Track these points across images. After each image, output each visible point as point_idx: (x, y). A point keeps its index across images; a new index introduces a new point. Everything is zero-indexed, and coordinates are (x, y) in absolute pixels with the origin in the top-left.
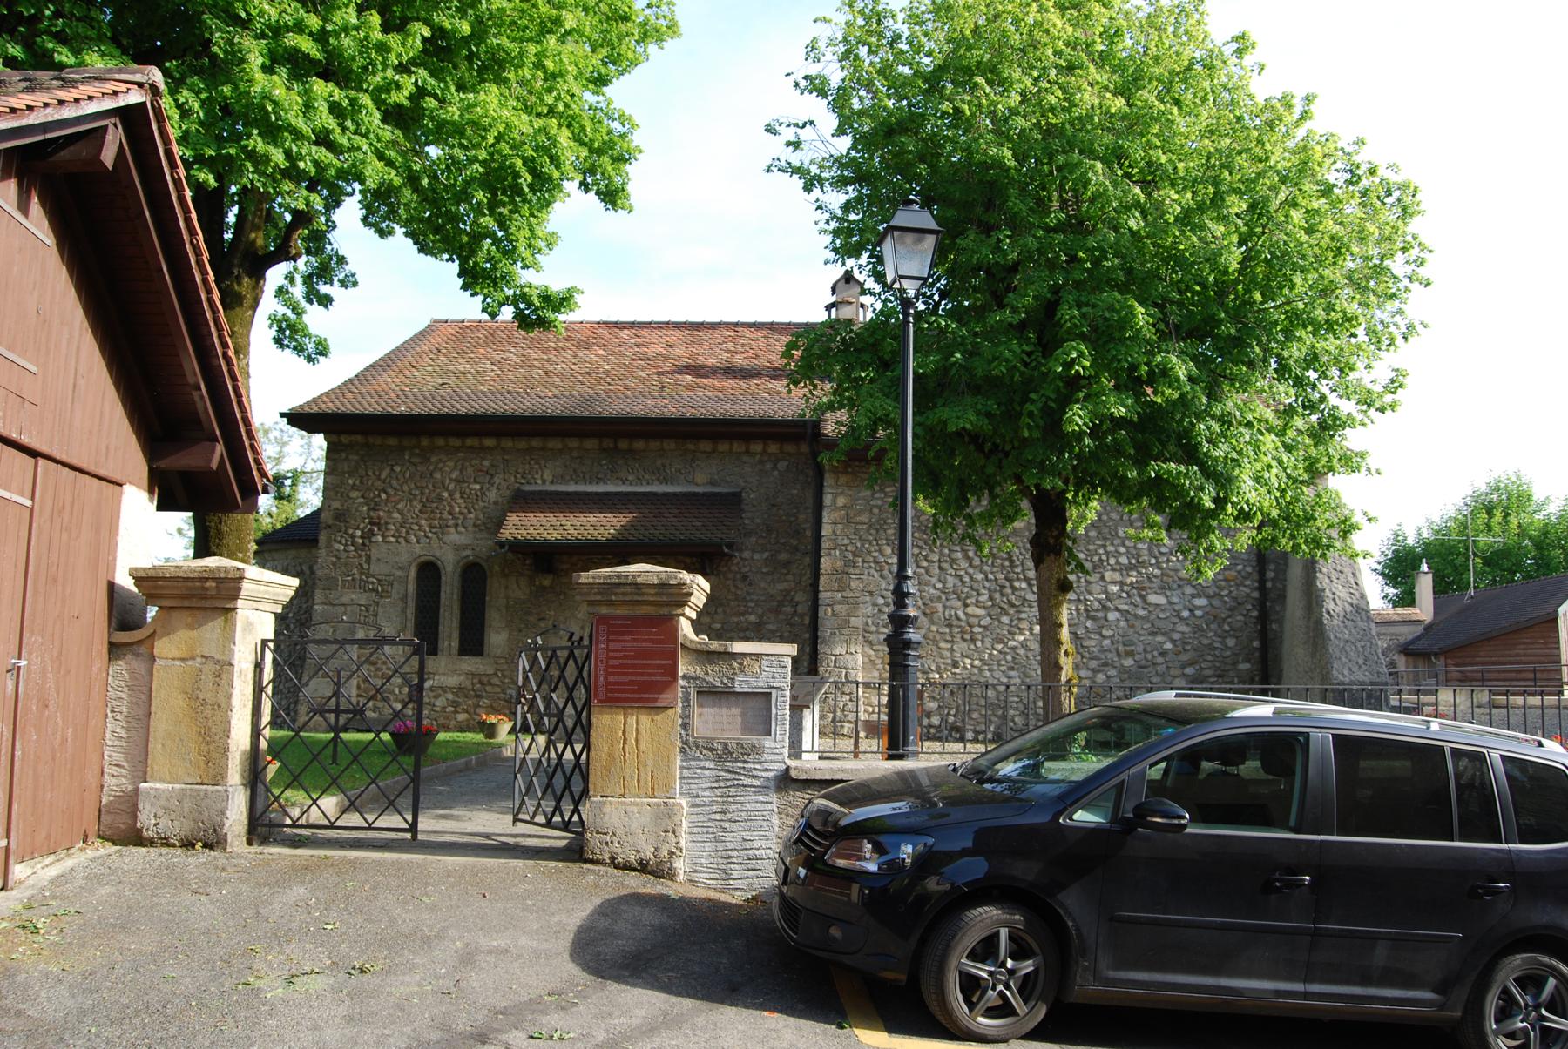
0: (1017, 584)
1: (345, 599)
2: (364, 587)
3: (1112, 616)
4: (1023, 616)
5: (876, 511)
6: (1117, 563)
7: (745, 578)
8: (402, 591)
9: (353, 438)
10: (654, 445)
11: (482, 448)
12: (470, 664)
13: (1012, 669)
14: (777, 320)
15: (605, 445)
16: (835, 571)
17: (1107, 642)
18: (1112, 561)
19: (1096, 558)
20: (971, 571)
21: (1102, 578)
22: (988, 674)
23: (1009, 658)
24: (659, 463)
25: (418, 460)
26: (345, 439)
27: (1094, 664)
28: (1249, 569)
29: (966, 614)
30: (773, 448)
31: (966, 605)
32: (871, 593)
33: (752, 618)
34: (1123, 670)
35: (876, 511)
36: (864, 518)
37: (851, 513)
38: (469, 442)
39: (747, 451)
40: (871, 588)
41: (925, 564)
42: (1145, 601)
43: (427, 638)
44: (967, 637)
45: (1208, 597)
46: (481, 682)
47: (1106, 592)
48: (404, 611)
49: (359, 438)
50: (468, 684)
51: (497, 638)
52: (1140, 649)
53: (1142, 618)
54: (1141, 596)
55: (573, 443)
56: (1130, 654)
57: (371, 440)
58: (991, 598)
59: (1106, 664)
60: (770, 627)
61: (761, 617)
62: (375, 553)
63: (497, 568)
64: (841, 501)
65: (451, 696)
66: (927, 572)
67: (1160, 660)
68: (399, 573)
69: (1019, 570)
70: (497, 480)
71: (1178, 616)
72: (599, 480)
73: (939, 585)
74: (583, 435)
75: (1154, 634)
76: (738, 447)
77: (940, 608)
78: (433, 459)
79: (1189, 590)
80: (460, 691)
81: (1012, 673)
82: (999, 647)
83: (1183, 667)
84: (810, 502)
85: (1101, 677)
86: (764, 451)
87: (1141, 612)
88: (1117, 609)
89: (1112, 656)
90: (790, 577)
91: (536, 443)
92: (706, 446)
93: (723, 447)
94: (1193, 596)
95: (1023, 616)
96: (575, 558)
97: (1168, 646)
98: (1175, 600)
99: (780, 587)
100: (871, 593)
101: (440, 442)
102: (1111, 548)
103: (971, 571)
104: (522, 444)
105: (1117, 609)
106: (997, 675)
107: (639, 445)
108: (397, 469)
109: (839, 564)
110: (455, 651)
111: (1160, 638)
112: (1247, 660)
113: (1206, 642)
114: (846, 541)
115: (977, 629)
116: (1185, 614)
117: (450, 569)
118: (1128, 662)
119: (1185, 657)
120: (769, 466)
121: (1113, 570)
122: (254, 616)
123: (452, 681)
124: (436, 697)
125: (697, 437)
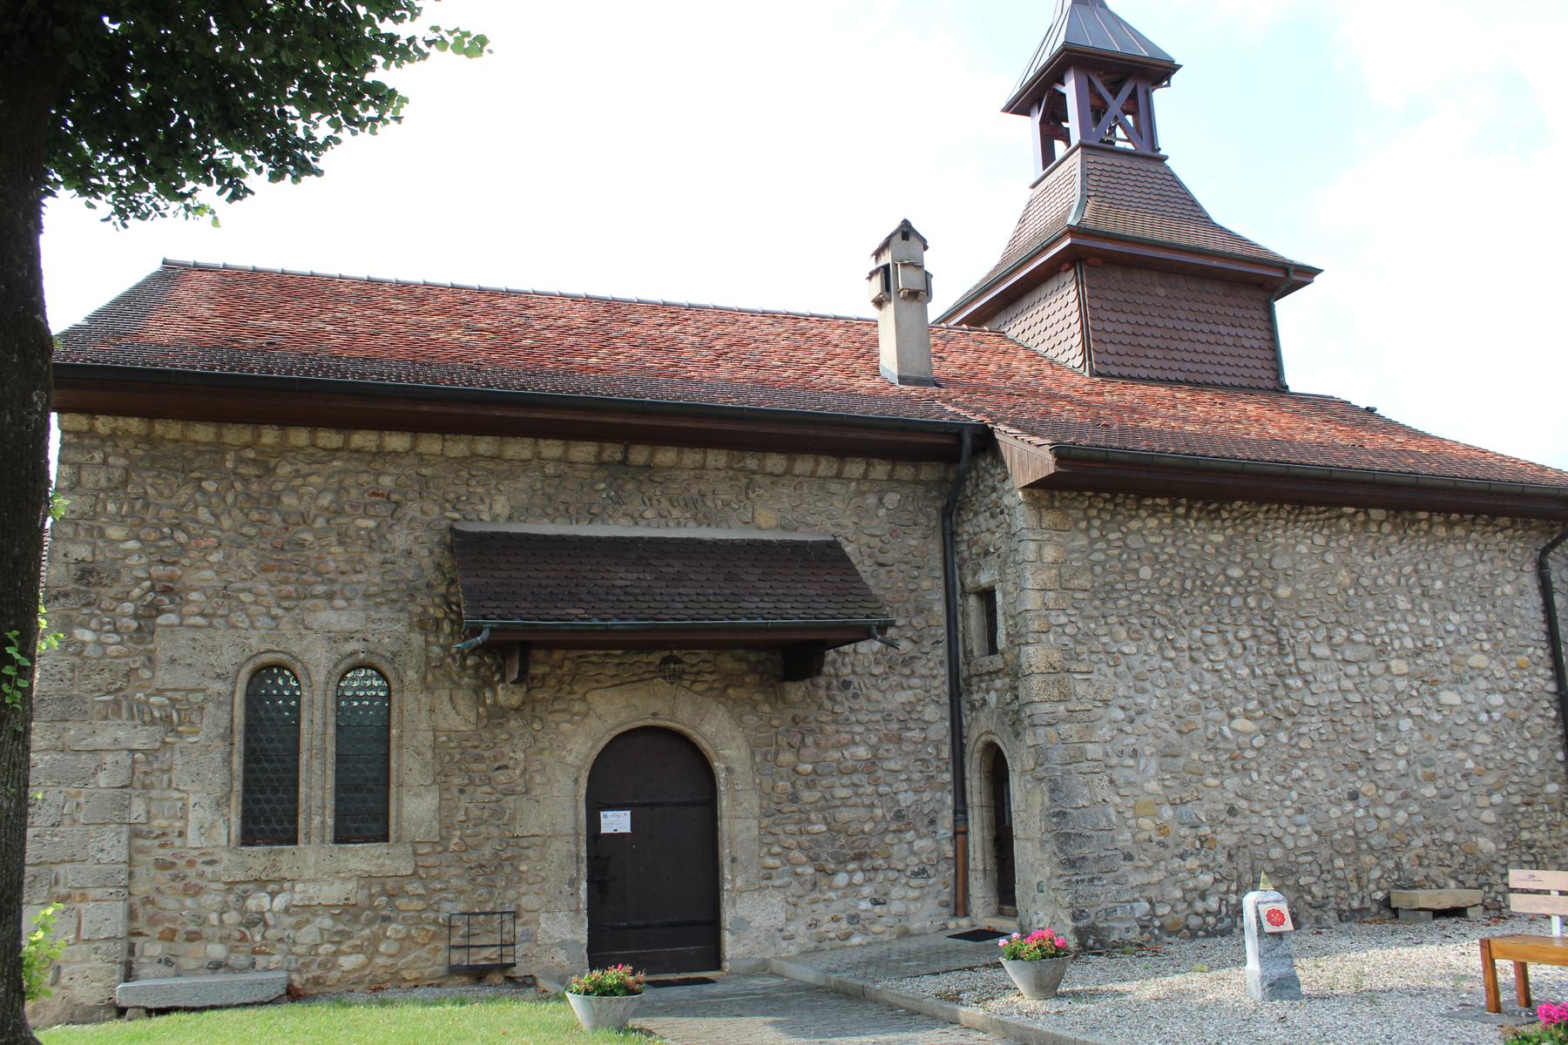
0: (1290, 682)
1: (103, 739)
2: (140, 714)
3: (1405, 724)
4: (1304, 730)
5: (1098, 569)
6: (1402, 647)
7: (846, 685)
8: (224, 721)
9: (121, 422)
10: (691, 457)
11: (380, 453)
12: (363, 857)
13: (1301, 811)
14: (261, 265)
15: (606, 456)
16: (1053, 669)
17: (1402, 764)
18: (1397, 644)
19: (1378, 641)
20: (1231, 663)
21: (1388, 669)
22: (1270, 822)
23: (1294, 795)
24: (694, 490)
25: (252, 471)
26: (103, 424)
27: (1391, 797)
28: (1540, 652)
29: (1233, 731)
30: (880, 470)
31: (1232, 717)
32: (1106, 703)
33: (862, 752)
34: (1426, 804)
35: (1098, 569)
36: (1083, 581)
37: (1066, 572)
38: (360, 439)
39: (838, 476)
40: (1105, 694)
41: (1172, 654)
42: (1438, 702)
43: (267, 816)
44: (1238, 766)
45: (1504, 692)
46: (384, 892)
47: (1393, 688)
48: (228, 761)
49: (135, 425)
50: (361, 897)
51: (415, 806)
52: (1440, 772)
53: (1438, 725)
54: (1433, 694)
55: (552, 449)
56: (1432, 778)
57: (159, 428)
58: (1262, 704)
59: (1405, 796)
60: (892, 765)
61: (874, 749)
62: (162, 646)
63: (411, 675)
64: (1050, 554)
65: (327, 923)
66: (1176, 666)
67: (1464, 786)
68: (218, 686)
69: (1290, 660)
70: (412, 509)
71: (1475, 721)
72: (593, 518)
73: (1195, 687)
74: (568, 433)
75: (1453, 747)
76: (826, 466)
77: (1201, 724)
78: (285, 469)
79: (1483, 684)
80: (347, 911)
81: (1301, 819)
82: (1280, 779)
83: (1489, 794)
84: (937, 562)
85: (1401, 817)
86: (865, 476)
87: (1437, 718)
88: (1409, 714)
89: (1409, 782)
90: (915, 682)
91: (485, 445)
92: (775, 462)
93: (803, 465)
94: (1489, 692)
95: (1304, 730)
96: (558, 655)
97: (1470, 764)
98: (1471, 698)
99: (904, 696)
100: (1106, 703)
101: (300, 437)
102: (1392, 626)
103: (1231, 663)
104: (458, 447)
105: (1409, 714)
106: (1284, 822)
107: (666, 456)
108: (210, 486)
109: (1056, 657)
110: (330, 835)
111: (1460, 754)
112: (1553, 780)
113: (1508, 756)
114: (1063, 619)
115: (1250, 754)
116: (1484, 717)
117: (319, 677)
118: (1429, 791)
119: (1490, 779)
120: (871, 500)
121: (1399, 657)
122: (739, 825)
123: (332, 892)
124: (298, 926)
125: (764, 445)
